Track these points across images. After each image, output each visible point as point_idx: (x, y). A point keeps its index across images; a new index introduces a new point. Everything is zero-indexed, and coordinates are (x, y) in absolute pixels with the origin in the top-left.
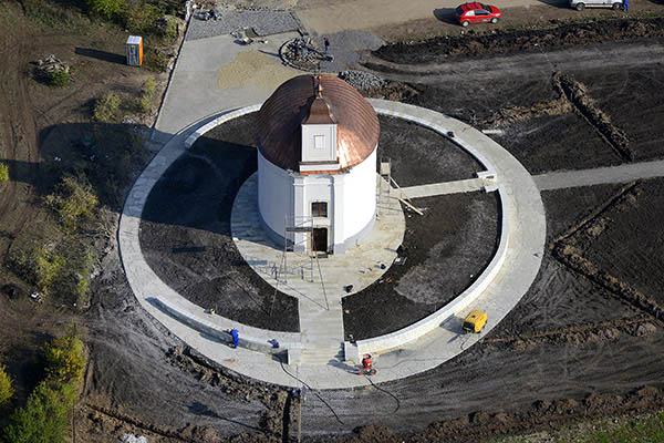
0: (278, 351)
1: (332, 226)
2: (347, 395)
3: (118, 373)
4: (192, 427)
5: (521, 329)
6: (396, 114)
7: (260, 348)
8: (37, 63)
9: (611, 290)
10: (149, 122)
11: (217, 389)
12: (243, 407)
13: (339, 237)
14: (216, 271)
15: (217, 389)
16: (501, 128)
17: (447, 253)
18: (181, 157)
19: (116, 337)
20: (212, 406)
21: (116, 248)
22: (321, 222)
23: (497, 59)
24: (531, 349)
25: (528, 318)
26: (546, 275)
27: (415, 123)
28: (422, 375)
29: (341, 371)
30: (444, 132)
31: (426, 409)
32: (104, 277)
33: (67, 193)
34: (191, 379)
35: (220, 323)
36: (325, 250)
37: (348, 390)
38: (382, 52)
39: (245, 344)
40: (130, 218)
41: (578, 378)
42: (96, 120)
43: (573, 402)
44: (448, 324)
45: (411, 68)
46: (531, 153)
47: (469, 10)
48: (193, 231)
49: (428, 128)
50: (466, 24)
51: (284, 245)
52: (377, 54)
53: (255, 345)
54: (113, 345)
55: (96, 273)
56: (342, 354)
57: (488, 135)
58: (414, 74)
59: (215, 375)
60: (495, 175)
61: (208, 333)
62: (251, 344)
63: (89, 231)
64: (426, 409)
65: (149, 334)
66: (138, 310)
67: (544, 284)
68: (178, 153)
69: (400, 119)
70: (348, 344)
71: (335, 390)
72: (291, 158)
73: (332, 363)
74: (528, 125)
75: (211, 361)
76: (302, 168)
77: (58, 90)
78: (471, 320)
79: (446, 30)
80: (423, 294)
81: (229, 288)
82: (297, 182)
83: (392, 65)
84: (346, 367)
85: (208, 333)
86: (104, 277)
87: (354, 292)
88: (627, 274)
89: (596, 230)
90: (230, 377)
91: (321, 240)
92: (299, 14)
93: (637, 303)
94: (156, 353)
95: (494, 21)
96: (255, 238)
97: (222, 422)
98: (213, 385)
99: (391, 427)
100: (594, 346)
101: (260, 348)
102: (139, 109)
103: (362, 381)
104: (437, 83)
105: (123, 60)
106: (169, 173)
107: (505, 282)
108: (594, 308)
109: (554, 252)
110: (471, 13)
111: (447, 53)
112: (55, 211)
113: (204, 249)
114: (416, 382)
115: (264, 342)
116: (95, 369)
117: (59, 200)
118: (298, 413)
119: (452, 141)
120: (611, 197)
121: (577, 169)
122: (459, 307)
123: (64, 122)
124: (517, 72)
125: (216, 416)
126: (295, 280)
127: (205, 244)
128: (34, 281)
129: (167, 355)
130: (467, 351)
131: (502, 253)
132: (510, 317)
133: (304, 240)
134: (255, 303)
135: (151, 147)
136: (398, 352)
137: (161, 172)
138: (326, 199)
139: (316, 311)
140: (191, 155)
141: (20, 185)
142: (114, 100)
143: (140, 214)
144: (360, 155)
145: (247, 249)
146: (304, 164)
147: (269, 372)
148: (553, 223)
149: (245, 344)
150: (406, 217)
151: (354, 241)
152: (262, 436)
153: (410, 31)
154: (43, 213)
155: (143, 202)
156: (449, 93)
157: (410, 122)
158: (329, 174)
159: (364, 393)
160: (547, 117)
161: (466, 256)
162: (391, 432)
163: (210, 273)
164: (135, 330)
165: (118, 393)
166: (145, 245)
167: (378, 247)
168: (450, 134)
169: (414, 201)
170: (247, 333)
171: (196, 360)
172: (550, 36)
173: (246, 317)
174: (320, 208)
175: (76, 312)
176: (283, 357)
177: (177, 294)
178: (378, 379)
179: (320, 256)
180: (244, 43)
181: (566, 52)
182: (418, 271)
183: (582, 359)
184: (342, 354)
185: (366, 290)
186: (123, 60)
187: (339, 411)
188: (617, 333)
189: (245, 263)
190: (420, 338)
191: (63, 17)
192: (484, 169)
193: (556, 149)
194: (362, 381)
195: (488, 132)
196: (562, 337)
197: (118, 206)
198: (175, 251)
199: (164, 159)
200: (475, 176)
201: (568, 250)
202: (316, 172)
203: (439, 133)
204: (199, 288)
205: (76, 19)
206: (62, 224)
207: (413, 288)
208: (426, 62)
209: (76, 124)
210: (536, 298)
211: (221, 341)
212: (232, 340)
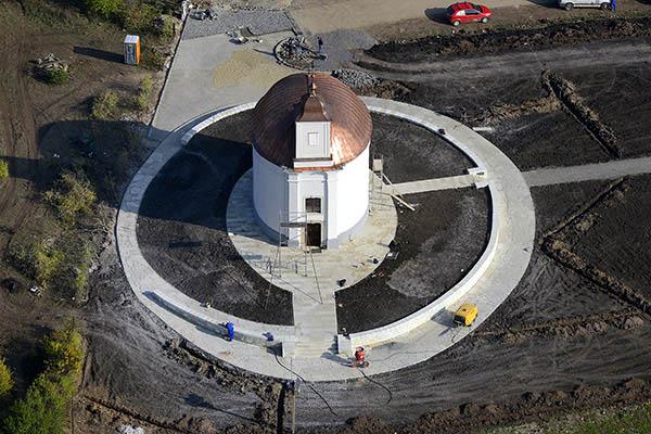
0: (272, 343)
1: (326, 222)
2: (340, 387)
3: (116, 366)
4: (188, 418)
5: (511, 322)
6: (388, 112)
7: (254, 341)
8: (36, 62)
9: (600, 284)
10: (146, 119)
11: (213, 381)
12: (239, 398)
13: (332, 233)
14: (212, 265)
15: (213, 381)
16: (491, 125)
17: (438, 248)
18: (178, 153)
19: (114, 330)
20: (208, 398)
21: (114, 243)
22: (314, 218)
23: (487, 58)
24: (521, 341)
25: (517, 311)
26: (535, 270)
27: (407, 120)
28: (413, 367)
29: (334, 363)
30: (436, 129)
31: (418, 401)
32: (102, 271)
33: (65, 189)
34: (187, 371)
35: (215, 317)
36: (319, 245)
37: (341, 382)
38: (374, 51)
39: (240, 337)
40: (127, 214)
41: (567, 370)
42: (94, 117)
43: (561, 394)
44: (439, 317)
45: (403, 67)
46: (521, 150)
47: (460, 9)
48: (189, 227)
49: (420, 125)
50: (456, 24)
51: (278, 240)
52: (369, 52)
53: (250, 338)
54: (111, 338)
55: (95, 267)
56: (335, 347)
57: (478, 132)
58: (406, 72)
59: (211, 368)
60: (485, 171)
61: (203, 327)
62: (246, 337)
63: (87, 226)
64: (418, 401)
65: (146, 327)
66: (135, 304)
67: (533, 278)
68: (175, 150)
69: (392, 117)
70: (341, 337)
71: (329, 382)
72: (285, 154)
73: (326, 355)
74: (518, 122)
75: (207, 354)
76: (296, 165)
77: (57, 88)
78: (462, 314)
79: (437, 29)
80: (415, 288)
81: (225, 282)
82: (291, 179)
83: (384, 64)
84: (339, 360)
85: (203, 327)
86: (102, 271)
87: (347, 286)
88: (615, 269)
89: (584, 225)
90: (226, 369)
91: (314, 235)
92: (293, 14)
93: (624, 297)
94: (153, 346)
95: (485, 20)
96: (250, 234)
97: (218, 413)
98: (209, 377)
99: (383, 418)
100: (583, 339)
101: (254, 341)
102: (136, 107)
103: (355, 373)
104: (428, 82)
105: (121, 59)
106: (166, 170)
107: (495, 276)
108: (582, 302)
109: (543, 247)
110: (461, 13)
111: (439, 52)
112: (53, 207)
113: (200, 244)
114: (408, 374)
115: (259, 335)
116: (94, 361)
117: (58, 196)
118: (292, 404)
119: (443, 138)
120: (599, 193)
121: (566, 166)
122: (450, 301)
123: (63, 119)
124: (507, 70)
125: (211, 407)
126: (290, 274)
127: (201, 239)
128: (33, 276)
129: (164, 348)
130: (458, 344)
131: (492, 248)
132: (500, 311)
133: (298, 235)
134: (250, 297)
135: (148, 144)
136: (390, 345)
137: (158, 169)
138: (320, 195)
139: (310, 305)
140: (187, 152)
141: (20, 181)
142: (111, 98)
143: (137, 210)
144: (353, 151)
145: (242, 244)
146: (299, 160)
147: (264, 365)
148: (543, 218)
149: (240, 337)
150: (398, 212)
151: (348, 236)
152: (256, 427)
153: (402, 30)
154: (42, 209)
155: (140, 198)
156: (440, 91)
157: (402, 120)
158: (323, 171)
159: (357, 385)
160: (537, 115)
161: (457, 251)
162: (383, 423)
163: (206, 267)
164: (132, 323)
165: (116, 385)
166: (142, 240)
167: (370, 242)
168: (442, 131)
169: (406, 197)
170: (242, 326)
171: (192, 352)
172: (539, 35)
173: (241, 311)
174: (313, 204)
175: (74, 305)
176: (277, 350)
177: (173, 288)
178: (370, 371)
179: (313, 251)
180: (239, 42)
181: (555, 51)
182: (410, 266)
183: (571, 352)
184: (335, 347)
185: (359, 285)
186: (121, 59)
187: (332, 403)
188: (605, 326)
189: (241, 258)
190: (411, 332)
191: (62, 17)
192: (475, 166)
193: (545, 146)
194: (355, 373)
195: (478, 129)
196: (551, 330)
197: (115, 202)
198: (171, 246)
199: (161, 155)
200: (466, 172)
201: (557, 244)
202: (310, 169)
203: (430, 130)
204: (195, 282)
205: (75, 18)
206: (60, 219)
207: (405, 282)
208: (417, 61)
209: (74, 121)
210: (526, 292)
211: (217, 334)
212: (228, 333)
